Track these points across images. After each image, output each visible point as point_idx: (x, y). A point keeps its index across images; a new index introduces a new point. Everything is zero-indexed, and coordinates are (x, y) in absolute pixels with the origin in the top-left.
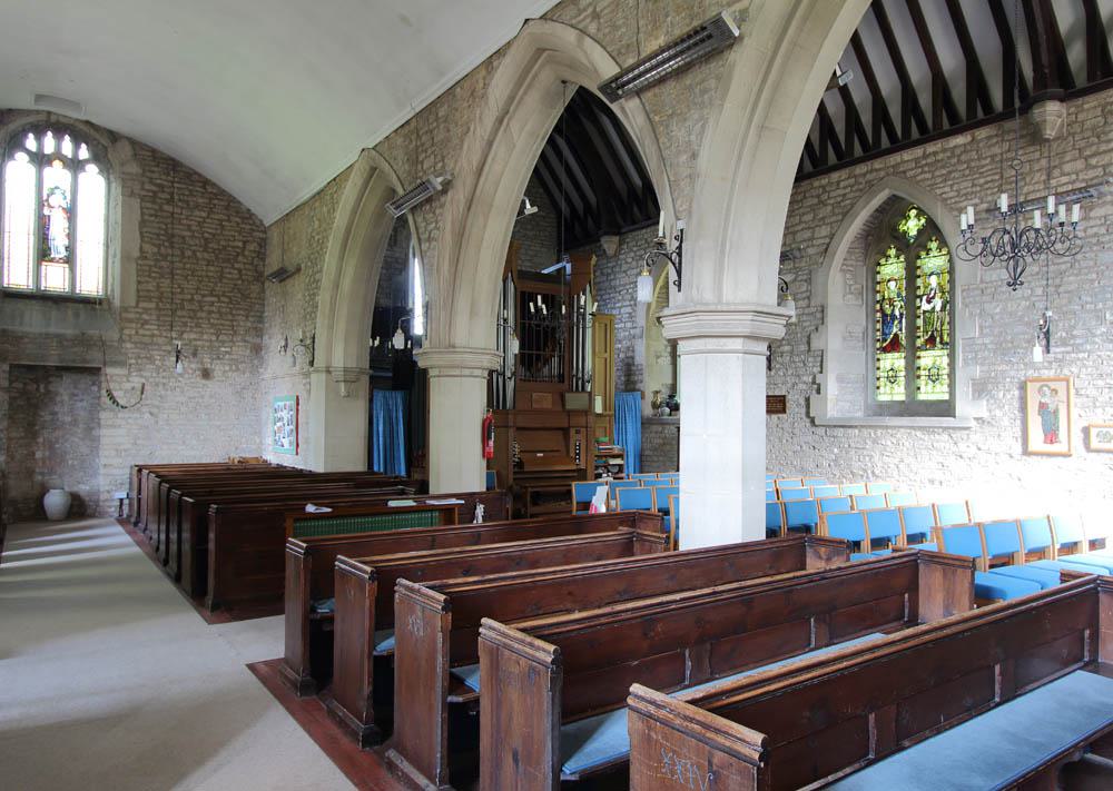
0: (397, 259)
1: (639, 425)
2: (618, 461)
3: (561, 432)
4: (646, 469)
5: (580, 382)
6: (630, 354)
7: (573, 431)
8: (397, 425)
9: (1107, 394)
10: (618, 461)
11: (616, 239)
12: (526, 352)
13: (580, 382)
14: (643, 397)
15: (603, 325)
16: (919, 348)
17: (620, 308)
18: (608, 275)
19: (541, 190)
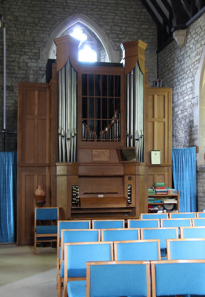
0: (40, 68)
1: (194, 172)
2: (173, 201)
3: (121, 179)
4: (198, 211)
5: (132, 141)
6: (191, 119)
7: (126, 178)
8: (8, 175)
9: (203, 33)
10: (173, 201)
11: (183, 32)
12: (108, 119)
13: (132, 141)
14: (197, 151)
15: (162, 97)
16: (137, 35)
17: (186, 85)
18: (181, 61)
19: (145, 10)
